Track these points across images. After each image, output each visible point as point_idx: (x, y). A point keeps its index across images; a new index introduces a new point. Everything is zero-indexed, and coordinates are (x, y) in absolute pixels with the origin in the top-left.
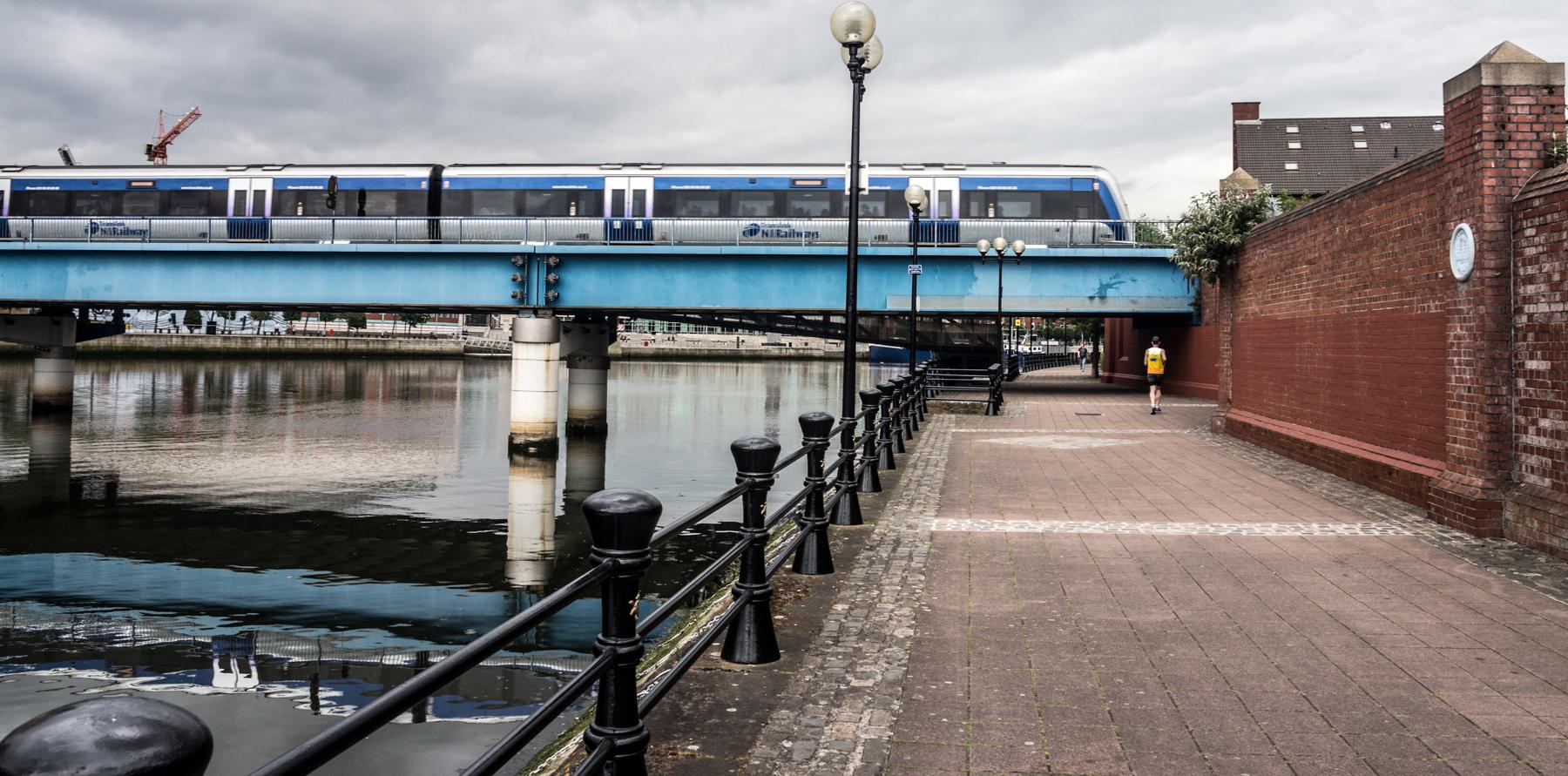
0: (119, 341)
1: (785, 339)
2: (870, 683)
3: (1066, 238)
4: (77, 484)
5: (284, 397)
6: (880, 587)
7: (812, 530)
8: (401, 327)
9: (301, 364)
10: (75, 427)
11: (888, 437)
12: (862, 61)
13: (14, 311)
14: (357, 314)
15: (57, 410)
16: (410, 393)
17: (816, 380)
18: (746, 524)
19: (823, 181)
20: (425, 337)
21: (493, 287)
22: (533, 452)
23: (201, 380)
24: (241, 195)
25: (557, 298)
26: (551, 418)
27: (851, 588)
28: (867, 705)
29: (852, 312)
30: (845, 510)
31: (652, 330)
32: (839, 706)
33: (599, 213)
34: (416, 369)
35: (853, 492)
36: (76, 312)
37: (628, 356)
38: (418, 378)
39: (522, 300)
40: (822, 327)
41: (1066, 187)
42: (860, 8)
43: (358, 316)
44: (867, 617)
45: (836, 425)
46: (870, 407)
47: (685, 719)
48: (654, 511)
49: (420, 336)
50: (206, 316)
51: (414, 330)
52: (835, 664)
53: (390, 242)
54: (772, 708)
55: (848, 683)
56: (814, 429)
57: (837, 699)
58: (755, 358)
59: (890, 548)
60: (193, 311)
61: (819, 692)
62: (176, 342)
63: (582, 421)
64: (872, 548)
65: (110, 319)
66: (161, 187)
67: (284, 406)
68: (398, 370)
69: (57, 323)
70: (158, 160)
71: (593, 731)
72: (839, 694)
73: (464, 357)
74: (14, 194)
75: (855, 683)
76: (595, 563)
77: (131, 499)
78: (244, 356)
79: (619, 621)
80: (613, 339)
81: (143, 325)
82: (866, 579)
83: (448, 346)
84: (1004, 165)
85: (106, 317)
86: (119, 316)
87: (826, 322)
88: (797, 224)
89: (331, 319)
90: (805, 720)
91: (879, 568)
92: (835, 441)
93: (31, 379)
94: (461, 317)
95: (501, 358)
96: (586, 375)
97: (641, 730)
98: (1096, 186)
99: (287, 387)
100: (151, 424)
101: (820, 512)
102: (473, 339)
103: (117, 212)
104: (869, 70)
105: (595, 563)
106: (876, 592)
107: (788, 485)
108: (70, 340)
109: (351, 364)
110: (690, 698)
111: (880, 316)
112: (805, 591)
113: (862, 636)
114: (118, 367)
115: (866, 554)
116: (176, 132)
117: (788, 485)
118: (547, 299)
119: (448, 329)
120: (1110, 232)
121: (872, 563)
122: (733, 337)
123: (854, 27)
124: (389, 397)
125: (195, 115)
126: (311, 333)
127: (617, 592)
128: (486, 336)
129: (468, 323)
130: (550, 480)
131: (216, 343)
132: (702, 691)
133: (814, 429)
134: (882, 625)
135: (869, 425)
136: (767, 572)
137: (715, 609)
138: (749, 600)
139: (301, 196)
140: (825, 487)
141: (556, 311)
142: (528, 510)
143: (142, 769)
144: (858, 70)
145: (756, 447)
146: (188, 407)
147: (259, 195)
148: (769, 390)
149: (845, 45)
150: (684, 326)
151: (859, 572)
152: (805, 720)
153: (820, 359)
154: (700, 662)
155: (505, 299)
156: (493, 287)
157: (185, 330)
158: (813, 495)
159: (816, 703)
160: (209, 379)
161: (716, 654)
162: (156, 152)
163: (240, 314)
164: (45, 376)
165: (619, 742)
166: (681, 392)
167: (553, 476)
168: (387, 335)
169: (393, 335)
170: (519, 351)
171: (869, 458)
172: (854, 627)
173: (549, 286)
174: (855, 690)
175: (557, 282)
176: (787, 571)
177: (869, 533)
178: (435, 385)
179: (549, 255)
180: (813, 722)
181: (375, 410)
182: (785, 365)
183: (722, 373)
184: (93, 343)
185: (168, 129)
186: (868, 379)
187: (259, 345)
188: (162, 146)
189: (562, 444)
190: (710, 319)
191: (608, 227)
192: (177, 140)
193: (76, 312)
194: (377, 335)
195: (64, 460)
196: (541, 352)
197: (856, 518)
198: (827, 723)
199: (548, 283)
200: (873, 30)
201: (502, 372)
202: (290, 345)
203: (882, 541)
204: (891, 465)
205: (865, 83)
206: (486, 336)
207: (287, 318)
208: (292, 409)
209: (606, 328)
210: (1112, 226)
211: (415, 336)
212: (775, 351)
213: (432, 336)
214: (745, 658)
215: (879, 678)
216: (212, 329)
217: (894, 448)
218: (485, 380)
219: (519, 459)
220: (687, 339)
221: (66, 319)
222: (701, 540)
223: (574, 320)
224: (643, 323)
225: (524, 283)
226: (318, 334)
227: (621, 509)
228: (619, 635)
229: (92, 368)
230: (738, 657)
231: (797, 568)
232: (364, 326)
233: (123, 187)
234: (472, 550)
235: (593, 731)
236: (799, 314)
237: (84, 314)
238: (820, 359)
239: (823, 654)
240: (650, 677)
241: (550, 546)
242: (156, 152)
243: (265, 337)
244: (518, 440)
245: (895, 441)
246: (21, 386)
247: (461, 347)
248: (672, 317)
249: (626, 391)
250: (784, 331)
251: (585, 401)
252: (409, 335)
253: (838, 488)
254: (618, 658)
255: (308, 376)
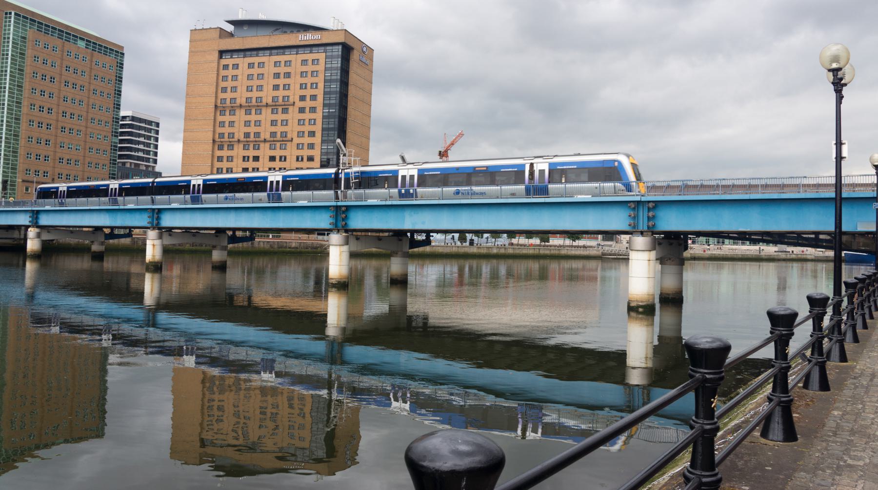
0: (427, 249)
1: (790, 249)
2: (861, 463)
3: (597, 191)
4: (410, 318)
5: (507, 278)
6: (862, 403)
7: (816, 364)
8: (568, 242)
9: (517, 261)
10: (409, 290)
11: (863, 309)
12: (841, 79)
13: (381, 234)
14: (544, 235)
15: (401, 282)
16: (572, 278)
17: (809, 273)
18: (776, 358)
19: (487, 167)
20: (581, 247)
21: (616, 220)
22: (642, 311)
23: (467, 269)
24: (404, 177)
25: (654, 226)
26: (651, 292)
27: (843, 401)
28: (861, 477)
29: (839, 232)
30: (836, 353)
31: (708, 243)
32: (840, 475)
33: (396, 186)
34: (577, 264)
35: (841, 343)
36: (409, 234)
37: (694, 258)
38: (577, 270)
39: (634, 227)
40: (814, 240)
41: (600, 165)
42: (839, 47)
43: (545, 236)
44: (855, 421)
45: (830, 301)
46: (850, 291)
47: (739, 470)
48: (727, 349)
49: (578, 247)
50: (469, 236)
51: (575, 244)
52: (836, 448)
53: (498, 198)
54: (795, 470)
55: (845, 461)
56: (817, 304)
57: (838, 470)
58: (770, 259)
59: (868, 379)
60: (462, 233)
61: (826, 464)
62: (455, 250)
63: (668, 294)
64: (855, 378)
65: (424, 238)
66: (490, 170)
67: (508, 283)
68: (566, 264)
69: (401, 240)
70: (444, 158)
71: (689, 471)
72: (839, 467)
73: (601, 258)
74: (419, 176)
75: (850, 462)
76: (691, 377)
77: (434, 327)
78: (488, 257)
79: (705, 410)
80: (686, 248)
81: (439, 241)
82: (853, 397)
83: (593, 252)
84: (579, 154)
85: (422, 237)
86: (428, 236)
87: (817, 238)
88: (476, 189)
89: (531, 238)
90: (817, 481)
91: (861, 391)
92: (830, 311)
93: (389, 268)
94: (600, 236)
95: (624, 259)
96: (671, 269)
97: (716, 475)
98: (616, 164)
99: (509, 274)
100: (443, 288)
101: (821, 353)
102: (607, 248)
103: (469, 183)
104: (845, 85)
105: (691, 377)
106: (860, 406)
107: (802, 335)
108: (406, 248)
109: (542, 262)
110: (742, 458)
111: (853, 234)
112: (812, 401)
113: (852, 432)
114: (427, 262)
115: (851, 381)
116: (452, 144)
117: (802, 335)
118: (648, 227)
119: (593, 243)
120: (624, 188)
121: (856, 387)
122: (756, 247)
123: (836, 59)
124: (562, 279)
125: (461, 135)
126: (521, 245)
127: (705, 393)
128: (612, 247)
129: (604, 240)
130: (650, 328)
131: (474, 250)
132: (749, 455)
133: (817, 304)
134: (867, 427)
135: (850, 302)
136: (790, 386)
137: (751, 407)
138: (780, 403)
139: (563, 172)
140: (823, 338)
141: (653, 233)
142: (638, 344)
143: (474, 468)
144: (839, 85)
145: (782, 313)
146: (461, 283)
147: (412, 177)
148: (779, 278)
149: (829, 70)
150: (727, 241)
151: (847, 392)
152: (817, 481)
153: (812, 260)
154: (748, 439)
155: (625, 227)
156: (616, 220)
157: (459, 243)
158: (816, 345)
159: (824, 471)
160: (471, 269)
161: (757, 434)
162: (443, 154)
163: (485, 235)
164: (395, 266)
165: (704, 480)
166: (725, 279)
167: (652, 324)
168: (560, 246)
169: (564, 246)
170: (633, 255)
171: (850, 322)
172: (847, 426)
173: (649, 219)
174: (850, 466)
175: (654, 217)
176: (799, 388)
177: (853, 368)
178: (586, 273)
179: (649, 202)
180: (823, 483)
181: (555, 286)
182: (790, 264)
183: (749, 267)
184: (416, 250)
185: (449, 143)
186: (852, 273)
187: (495, 251)
188: (446, 151)
189: (658, 306)
190: (743, 237)
191: (400, 192)
192: (453, 148)
193: (409, 234)
194: (555, 246)
195: (404, 308)
196: (645, 256)
197: (843, 358)
198: (832, 485)
199: (648, 217)
200: (848, 59)
201: (622, 267)
202: (510, 251)
203: (862, 374)
204: (865, 326)
205: (843, 93)
206: (612, 247)
207: (509, 237)
208: (511, 285)
209: (682, 242)
210: (624, 185)
211: (575, 247)
212: (783, 256)
213: (584, 247)
214: (775, 438)
215: (867, 461)
216: (472, 242)
217: (867, 316)
218: (613, 271)
219: (633, 314)
220: (729, 248)
221: (404, 239)
222: (750, 366)
223: (663, 238)
224: (703, 239)
225: (635, 218)
226: (525, 245)
227: (707, 346)
228: (706, 418)
229: (416, 262)
230: (771, 437)
231: (806, 386)
232: (548, 242)
233: (471, 171)
234: (611, 364)
235: (689, 471)
236: (799, 234)
237: (412, 236)
238: (812, 260)
239: (826, 441)
240: (720, 446)
241: (650, 365)
242: (443, 154)
243: (498, 247)
244: (632, 304)
245: (867, 311)
246: (385, 270)
247: (599, 253)
248: (720, 236)
249: (694, 278)
250: (789, 244)
251: (670, 284)
252: (572, 246)
253: (831, 340)
254: (705, 431)
255: (521, 267)
